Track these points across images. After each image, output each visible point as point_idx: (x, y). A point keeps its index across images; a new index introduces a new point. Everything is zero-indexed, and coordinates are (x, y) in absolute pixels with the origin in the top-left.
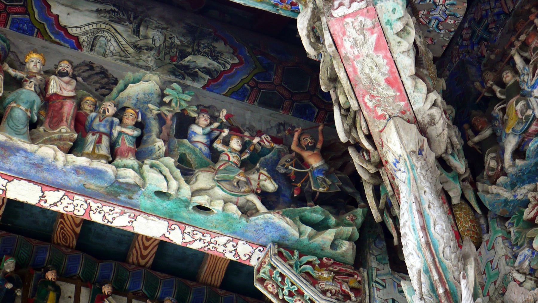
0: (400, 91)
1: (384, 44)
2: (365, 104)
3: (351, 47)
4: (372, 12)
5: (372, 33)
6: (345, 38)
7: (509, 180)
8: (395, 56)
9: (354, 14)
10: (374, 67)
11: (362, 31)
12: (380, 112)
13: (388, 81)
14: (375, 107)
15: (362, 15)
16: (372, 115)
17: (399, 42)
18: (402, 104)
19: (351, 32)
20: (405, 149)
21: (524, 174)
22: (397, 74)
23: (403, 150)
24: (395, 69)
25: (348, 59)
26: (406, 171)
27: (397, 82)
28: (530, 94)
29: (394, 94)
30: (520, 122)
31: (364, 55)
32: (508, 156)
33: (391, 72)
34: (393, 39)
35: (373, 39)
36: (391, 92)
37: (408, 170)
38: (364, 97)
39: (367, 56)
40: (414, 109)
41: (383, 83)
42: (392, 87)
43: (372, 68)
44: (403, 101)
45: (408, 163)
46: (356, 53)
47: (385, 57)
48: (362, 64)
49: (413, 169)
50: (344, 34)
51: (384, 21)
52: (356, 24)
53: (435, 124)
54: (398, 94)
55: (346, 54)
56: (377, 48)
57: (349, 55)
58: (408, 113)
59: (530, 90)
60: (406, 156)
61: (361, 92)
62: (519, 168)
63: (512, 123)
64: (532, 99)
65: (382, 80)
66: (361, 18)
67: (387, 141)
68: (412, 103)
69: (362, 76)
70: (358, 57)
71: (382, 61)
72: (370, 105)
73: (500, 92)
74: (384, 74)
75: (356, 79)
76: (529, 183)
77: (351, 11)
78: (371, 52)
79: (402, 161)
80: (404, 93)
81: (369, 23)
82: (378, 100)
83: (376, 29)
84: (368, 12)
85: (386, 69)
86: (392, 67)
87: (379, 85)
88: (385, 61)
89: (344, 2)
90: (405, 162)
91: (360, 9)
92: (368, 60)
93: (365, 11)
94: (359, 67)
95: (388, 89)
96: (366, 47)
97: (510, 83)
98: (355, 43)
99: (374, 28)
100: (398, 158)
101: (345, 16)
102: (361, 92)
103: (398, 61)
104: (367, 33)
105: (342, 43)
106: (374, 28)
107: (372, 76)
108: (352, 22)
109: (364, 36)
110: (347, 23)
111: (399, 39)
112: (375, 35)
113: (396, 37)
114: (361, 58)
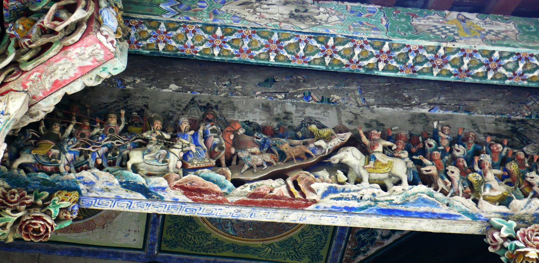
0: (51, 90)
1: (85, 71)
2: (32, 74)
3: (77, 53)
4: (109, 57)
5: (92, 62)
6: (83, 48)
7: (7, 173)
8: (79, 80)
9: (104, 47)
10: (65, 70)
11: (92, 55)
12: (28, 84)
13: (56, 82)
14: (32, 80)
15: (105, 52)
16: (24, 81)
17: (91, 79)
18: (41, 95)
19: (89, 50)
20: (16, 115)
21: (15, 179)
22: (64, 85)
23: (15, 114)
24: (68, 82)
25: (66, 54)
26: (3, 124)
27: (58, 87)
28: (65, 153)
29: (47, 88)
30: (46, 156)
31: (73, 62)
32: (19, 162)
33: (65, 81)
34: (93, 74)
35: (88, 63)
36: (48, 86)
37: (4, 125)
38: (37, 71)
39: (73, 64)
40: (40, 103)
41: (54, 79)
42: (53, 85)
43: (64, 69)
44: (44, 94)
45: (8, 122)
46: (73, 57)
47: (76, 74)
48: (65, 63)
49: (7, 127)
50: (86, 46)
51: (105, 66)
52: (97, 51)
53: (31, 118)
54: (48, 90)
55: (70, 52)
56: (81, 68)
57: (69, 54)
58: (34, 100)
59: (66, 150)
60: (12, 118)
61: (41, 69)
62: (19, 175)
63: (41, 152)
64: (64, 156)
65: (57, 77)
66: (102, 52)
67: (12, 99)
68: (44, 100)
69: (55, 66)
70: (70, 59)
71: (72, 74)
72: (32, 77)
73: (43, 128)
74: (61, 78)
75: (51, 63)
76: (9, 184)
77: (106, 45)
78: (77, 66)
79: (7, 117)
80: (51, 93)
81: (100, 58)
82: (38, 81)
83: (96, 63)
84: (109, 55)
85: (66, 77)
86: (69, 80)
87: (51, 77)
88: (73, 75)
89: (109, 37)
90: (8, 119)
91: (110, 50)
92: (70, 66)
93: (109, 53)
94: (62, 61)
95: (50, 83)
96: (80, 61)
97: (55, 132)
98: (79, 55)
99: (97, 61)
100: (6, 113)
101: (100, 43)
102: (41, 69)
103: (76, 82)
104: (92, 59)
105: (78, 47)
106: (97, 61)
107: (57, 71)
108: (97, 48)
109: (88, 58)
110: (96, 46)
111: (93, 78)
112: (92, 64)
113: (95, 75)
114: (69, 61)
